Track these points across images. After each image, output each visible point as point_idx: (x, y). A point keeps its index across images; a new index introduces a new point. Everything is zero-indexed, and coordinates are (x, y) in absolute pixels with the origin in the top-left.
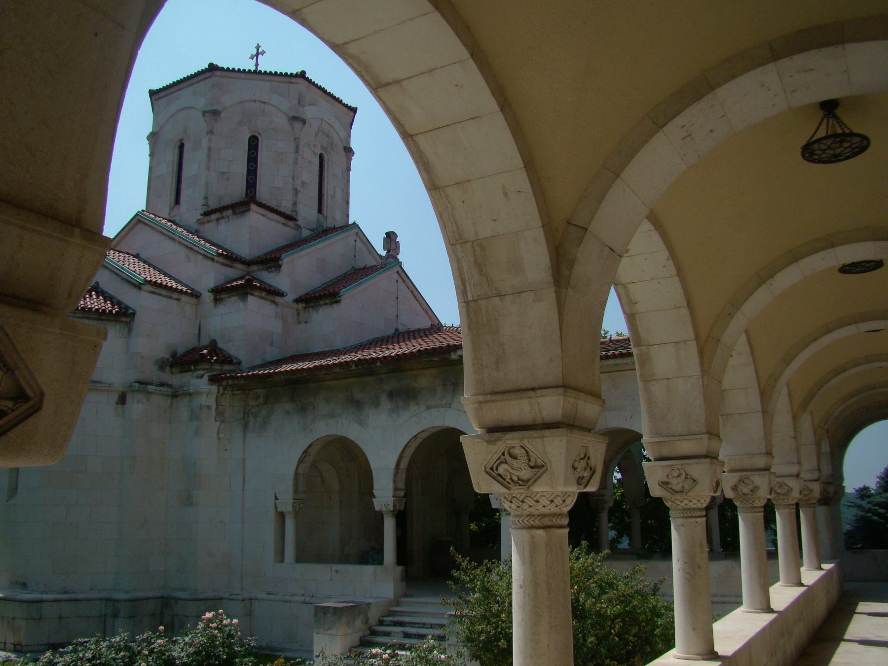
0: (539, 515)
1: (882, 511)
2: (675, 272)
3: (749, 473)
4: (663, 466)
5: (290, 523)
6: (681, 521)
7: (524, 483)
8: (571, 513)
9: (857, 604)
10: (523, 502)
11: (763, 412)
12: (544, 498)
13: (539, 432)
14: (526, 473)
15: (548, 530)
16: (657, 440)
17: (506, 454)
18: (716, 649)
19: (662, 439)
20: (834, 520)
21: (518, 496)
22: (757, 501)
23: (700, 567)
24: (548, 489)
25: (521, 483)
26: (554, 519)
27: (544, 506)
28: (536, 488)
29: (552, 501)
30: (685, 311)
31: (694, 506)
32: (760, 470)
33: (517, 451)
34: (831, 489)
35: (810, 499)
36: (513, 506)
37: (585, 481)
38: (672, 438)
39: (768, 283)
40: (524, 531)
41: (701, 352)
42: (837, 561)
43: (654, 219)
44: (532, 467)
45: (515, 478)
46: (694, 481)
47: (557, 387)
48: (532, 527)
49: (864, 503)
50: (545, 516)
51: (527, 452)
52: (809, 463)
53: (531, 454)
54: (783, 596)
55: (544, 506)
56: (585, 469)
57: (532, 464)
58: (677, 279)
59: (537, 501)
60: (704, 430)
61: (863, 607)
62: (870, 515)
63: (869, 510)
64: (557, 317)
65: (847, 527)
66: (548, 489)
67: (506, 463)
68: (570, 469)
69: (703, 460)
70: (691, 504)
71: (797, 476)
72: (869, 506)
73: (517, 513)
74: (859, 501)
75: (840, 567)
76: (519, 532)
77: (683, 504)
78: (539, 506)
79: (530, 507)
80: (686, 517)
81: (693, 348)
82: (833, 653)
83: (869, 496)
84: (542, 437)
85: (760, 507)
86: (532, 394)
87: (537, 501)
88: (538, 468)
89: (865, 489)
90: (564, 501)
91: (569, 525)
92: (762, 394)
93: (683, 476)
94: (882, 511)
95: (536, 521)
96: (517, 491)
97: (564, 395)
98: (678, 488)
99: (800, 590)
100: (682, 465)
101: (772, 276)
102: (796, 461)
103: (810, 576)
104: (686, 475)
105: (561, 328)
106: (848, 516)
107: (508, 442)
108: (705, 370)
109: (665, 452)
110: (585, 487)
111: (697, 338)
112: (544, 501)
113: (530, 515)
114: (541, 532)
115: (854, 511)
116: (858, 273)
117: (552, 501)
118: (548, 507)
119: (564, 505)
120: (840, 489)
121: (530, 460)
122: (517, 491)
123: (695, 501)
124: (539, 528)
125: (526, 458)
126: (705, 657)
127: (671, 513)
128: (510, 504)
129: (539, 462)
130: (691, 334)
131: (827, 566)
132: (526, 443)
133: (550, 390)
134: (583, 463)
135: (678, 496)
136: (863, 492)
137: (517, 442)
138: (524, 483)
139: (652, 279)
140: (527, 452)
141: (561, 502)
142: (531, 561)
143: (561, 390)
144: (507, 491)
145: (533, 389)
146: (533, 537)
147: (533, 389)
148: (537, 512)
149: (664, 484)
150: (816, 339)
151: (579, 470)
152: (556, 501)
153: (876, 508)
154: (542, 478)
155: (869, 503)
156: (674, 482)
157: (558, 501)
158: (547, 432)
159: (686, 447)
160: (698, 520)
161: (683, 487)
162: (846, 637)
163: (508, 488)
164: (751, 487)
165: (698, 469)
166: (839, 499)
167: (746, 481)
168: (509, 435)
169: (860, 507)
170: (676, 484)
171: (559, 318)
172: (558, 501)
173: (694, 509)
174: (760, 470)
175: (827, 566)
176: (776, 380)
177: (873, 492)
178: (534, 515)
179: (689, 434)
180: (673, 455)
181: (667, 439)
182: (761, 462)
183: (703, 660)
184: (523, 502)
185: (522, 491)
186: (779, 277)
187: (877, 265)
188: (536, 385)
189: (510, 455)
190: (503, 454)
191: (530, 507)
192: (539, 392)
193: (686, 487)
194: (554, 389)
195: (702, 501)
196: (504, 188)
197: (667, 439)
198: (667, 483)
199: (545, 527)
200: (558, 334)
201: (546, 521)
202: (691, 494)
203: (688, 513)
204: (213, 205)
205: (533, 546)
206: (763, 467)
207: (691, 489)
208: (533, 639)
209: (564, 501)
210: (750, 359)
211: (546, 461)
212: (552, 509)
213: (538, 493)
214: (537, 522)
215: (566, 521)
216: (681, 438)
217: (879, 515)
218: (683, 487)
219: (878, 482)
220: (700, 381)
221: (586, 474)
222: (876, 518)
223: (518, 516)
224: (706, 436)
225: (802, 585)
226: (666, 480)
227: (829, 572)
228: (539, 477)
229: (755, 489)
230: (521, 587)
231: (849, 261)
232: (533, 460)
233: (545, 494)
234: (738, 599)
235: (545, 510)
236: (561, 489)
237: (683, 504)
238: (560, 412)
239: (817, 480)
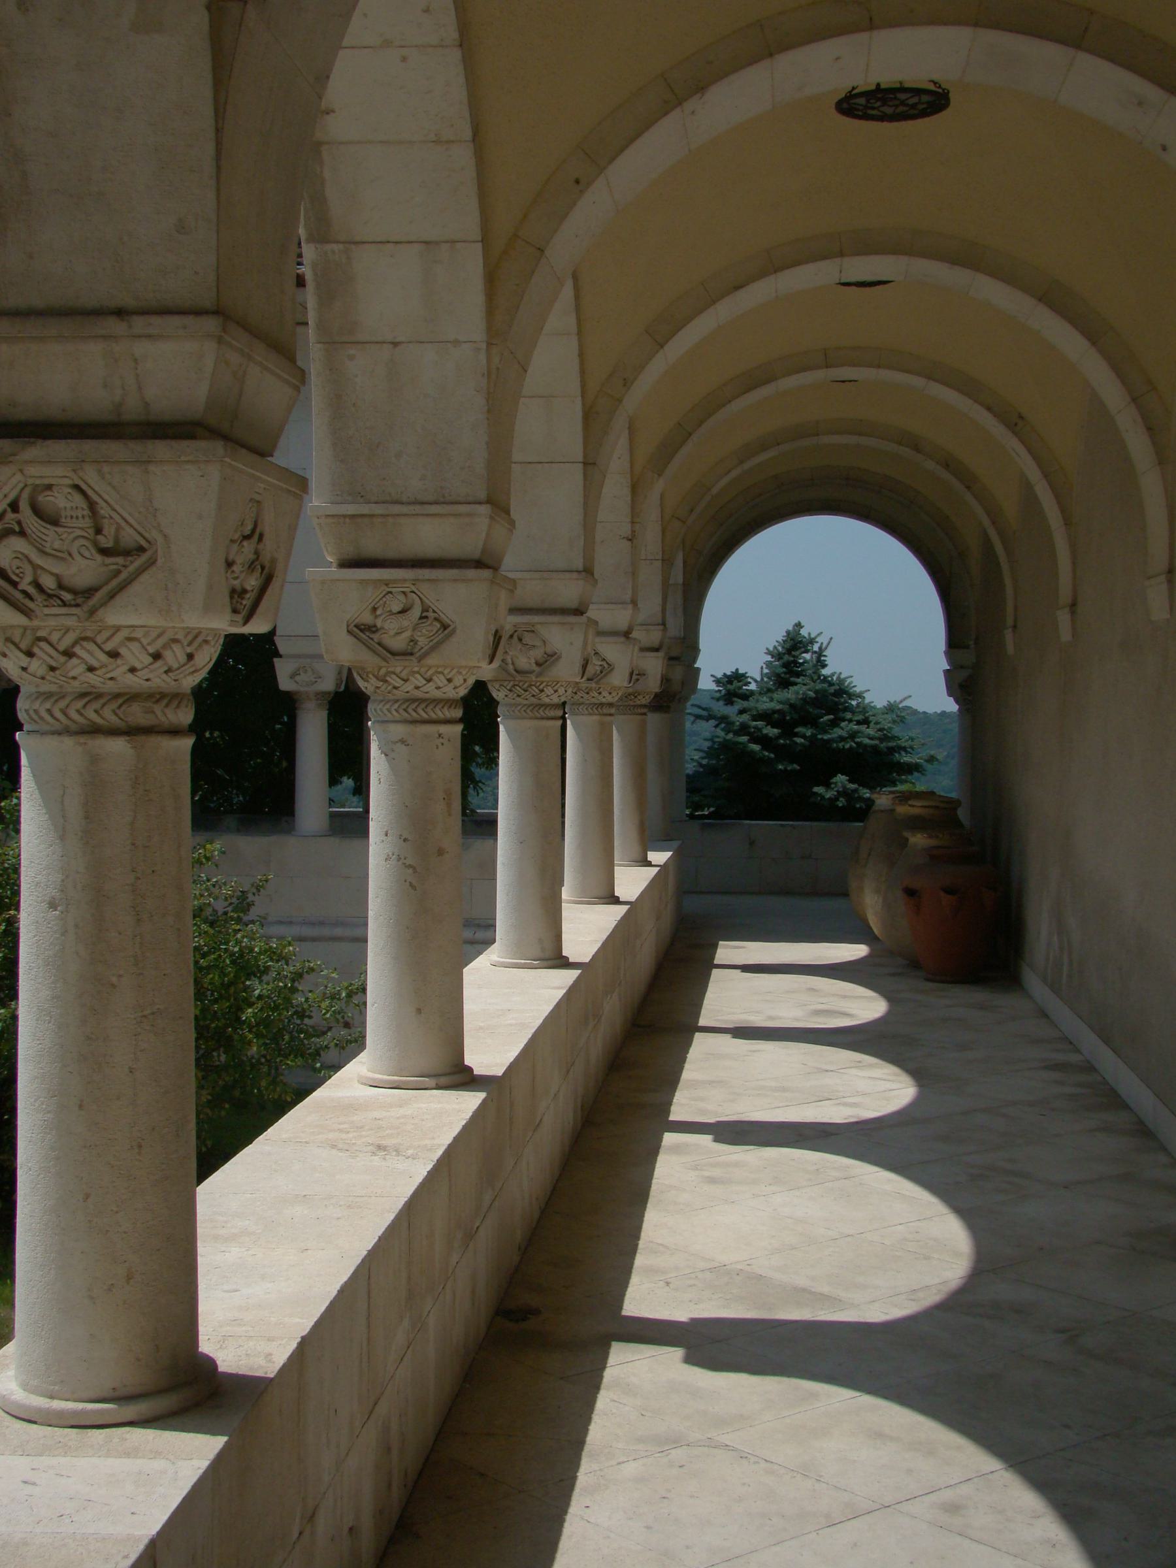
0: (117, 696)
1: (772, 732)
2: (452, 34)
3: (536, 619)
4: (363, 582)
5: (1010, 621)
6: (399, 730)
7: (82, 597)
8: (199, 693)
9: (715, 946)
10: (69, 654)
11: (585, 464)
12: (135, 646)
13: (136, 447)
14: (84, 569)
15: (141, 738)
16: (351, 509)
17: (24, 506)
18: (468, 1061)
19: (365, 509)
20: (674, 741)
21: (54, 638)
22: (549, 691)
23: (441, 852)
24: (152, 620)
25: (67, 597)
26: (158, 709)
27: (133, 670)
28: (114, 616)
29: (157, 656)
30: (463, 156)
31: (438, 694)
32: (564, 611)
33: (61, 500)
34: (678, 673)
35: (635, 695)
36: (35, 665)
37: (247, 601)
38: (396, 509)
39: (688, 106)
40: (68, 742)
41: (491, 279)
42: (676, 844)
43: (575, 277)
44: (104, 552)
45: (49, 583)
46: (445, 627)
47: (198, 312)
48: (95, 730)
49: (731, 711)
50: (133, 697)
51: (92, 506)
52: (651, 605)
53: (104, 511)
54: (586, 929)
55: (133, 670)
56: (251, 567)
57: (106, 542)
58: (457, 54)
59: (114, 655)
60: (482, 495)
61: (728, 951)
62: (744, 739)
63: (744, 729)
64: (207, 92)
65: (690, 768)
66: (152, 620)
67: (22, 533)
68: (221, 565)
69: (471, 573)
70: (430, 687)
71: (627, 634)
72: (745, 718)
73: (46, 687)
74: (721, 708)
75: (679, 856)
76: (52, 742)
77: (409, 687)
78: (119, 670)
79: (91, 669)
80: (414, 722)
81: (473, 263)
82: (682, 1060)
83: (746, 697)
84: (144, 463)
85: (450, 703)
86: (114, 325)
87: (114, 655)
88: (128, 556)
89: (737, 677)
90: (190, 657)
91: (195, 728)
92: (588, 416)
93: (416, 612)
94: (772, 732)
95: (107, 712)
96: (55, 622)
97: (220, 341)
98: (399, 643)
99: (616, 913)
100: (415, 582)
101: (700, 88)
102: (628, 597)
103: (632, 882)
104: (425, 609)
105: (218, 130)
106: (699, 737)
107: (32, 470)
108: (495, 334)
109: (372, 546)
110: (247, 621)
111: (485, 240)
112: (134, 655)
113: (89, 696)
114: (118, 746)
115: (706, 728)
116: (882, 118)
117: (157, 656)
118: (143, 674)
119: (189, 668)
120: (693, 674)
121: (99, 531)
122: (52, 622)
123: (440, 680)
124: (113, 732)
125: (87, 523)
126: (443, 1080)
127: (371, 708)
128: (24, 661)
129: (129, 537)
130: (470, 224)
131: (659, 857)
132: (90, 477)
133: (176, 320)
134: (248, 547)
135: (398, 665)
136: (733, 685)
137: (59, 471)
138: (82, 597)
139: (387, 44)
140: (92, 506)
141: (183, 659)
142: (85, 825)
143: (211, 324)
144: (19, 619)
145: (120, 313)
146: (95, 759)
147: (120, 313)
148: (110, 687)
149: (363, 631)
150: (737, 288)
151: (237, 568)
152: (167, 654)
153: (760, 724)
154: (136, 587)
155: (741, 712)
156: (390, 625)
157: (173, 657)
158: (161, 449)
159: (430, 534)
160: (443, 729)
161: (413, 641)
162: (702, 1022)
163: (26, 612)
164: (538, 653)
165: (455, 596)
166: (687, 699)
167: (527, 638)
168: (38, 450)
169: (723, 719)
170: (395, 633)
171: (216, 100)
172: (173, 657)
173: (436, 702)
174: (564, 611)
175: (659, 857)
176: (627, 383)
177: (753, 687)
178: (99, 696)
179: (440, 501)
180: (391, 554)
181: (378, 510)
182: (568, 591)
183: (438, 1087)
184: (69, 654)
185: (70, 622)
186: (718, 94)
187: (933, 101)
188: (129, 302)
189: (37, 511)
190: (14, 506)
191: (91, 669)
192: (139, 323)
193: (422, 641)
194: (189, 320)
195: (458, 680)
196: (34, 1484)
197: (378, 510)
198: (371, 629)
199: (131, 732)
200: (211, 148)
201: (137, 714)
202: (431, 661)
203: (417, 710)
204: (45, 597)
205: (95, 786)
206: (574, 604)
207: (433, 648)
208: (85, 1052)
209: (190, 657)
210: (572, 320)
211: (154, 535)
212: (158, 679)
213: (118, 629)
214: (109, 716)
215: (186, 716)
216: (417, 509)
217: (765, 741)
218: (413, 641)
219: (768, 664)
220: (483, 357)
221: (252, 583)
222: (756, 747)
223: (48, 696)
224: (484, 509)
225: (616, 901)
226: (367, 618)
227: (664, 868)
228: (122, 587)
229: (549, 659)
230: (53, 905)
231: (865, 81)
232: (109, 530)
233: (138, 634)
234: (488, 934)
235: (134, 682)
236: (194, 620)
237: (409, 687)
238: (201, 393)
239: (657, 650)
